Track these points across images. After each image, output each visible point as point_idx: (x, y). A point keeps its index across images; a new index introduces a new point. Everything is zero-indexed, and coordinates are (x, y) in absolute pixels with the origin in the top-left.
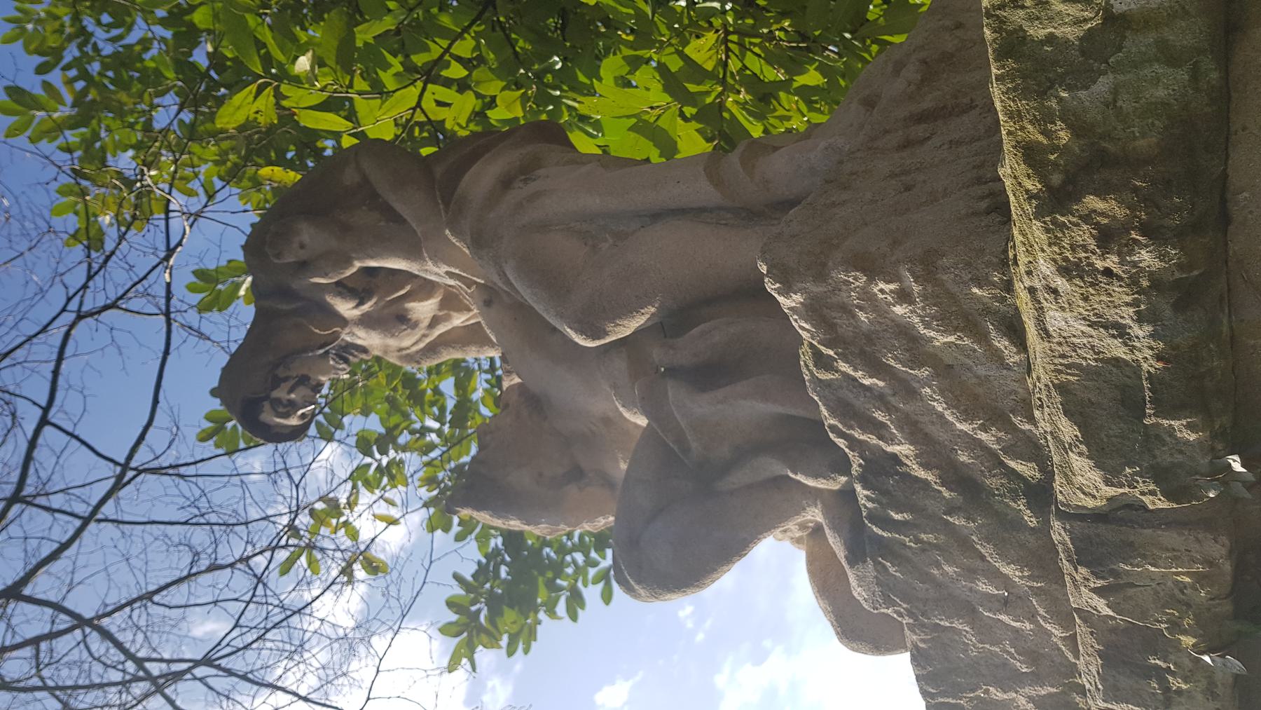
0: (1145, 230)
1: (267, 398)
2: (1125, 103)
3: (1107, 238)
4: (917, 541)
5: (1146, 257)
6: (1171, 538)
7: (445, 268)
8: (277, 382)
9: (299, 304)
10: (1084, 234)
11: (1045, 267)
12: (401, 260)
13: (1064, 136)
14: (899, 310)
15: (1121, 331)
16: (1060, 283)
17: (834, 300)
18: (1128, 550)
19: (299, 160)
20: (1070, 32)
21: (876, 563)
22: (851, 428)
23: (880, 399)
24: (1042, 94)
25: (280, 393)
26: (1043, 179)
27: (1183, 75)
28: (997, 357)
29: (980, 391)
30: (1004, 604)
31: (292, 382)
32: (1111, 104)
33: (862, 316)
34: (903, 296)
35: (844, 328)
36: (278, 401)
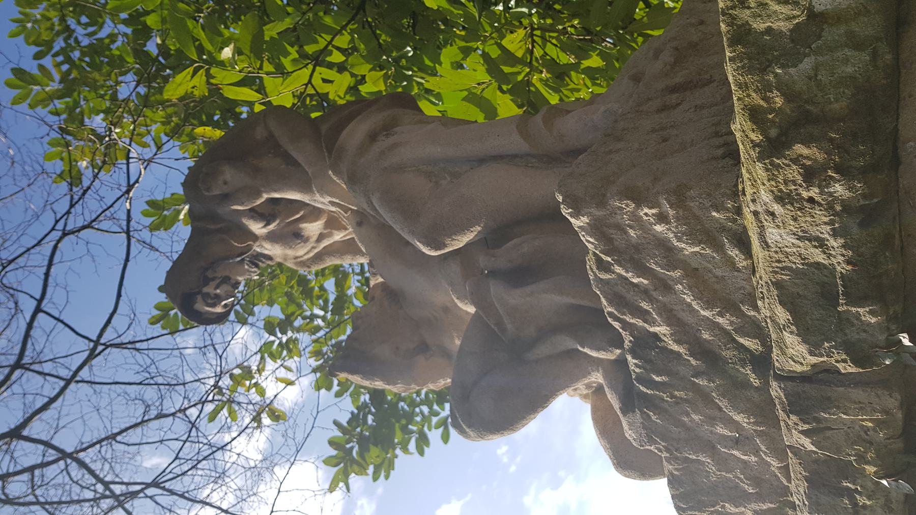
1: (199, 292)
2: (823, 77)
4: (672, 396)
5: (839, 189)
8: (206, 281)
10: (794, 173)
11: (765, 197)
12: (296, 193)
13: (779, 101)
14: (659, 228)
15: (821, 244)
16: (777, 208)
17: (612, 221)
18: (827, 403)
20: (783, 26)
21: (642, 413)
23: (645, 293)
24: (763, 70)
25: (209, 289)
26: (764, 132)
27: (866, 57)
29: (717, 287)
30: (736, 443)
31: (217, 281)
33: (632, 233)
34: (662, 218)
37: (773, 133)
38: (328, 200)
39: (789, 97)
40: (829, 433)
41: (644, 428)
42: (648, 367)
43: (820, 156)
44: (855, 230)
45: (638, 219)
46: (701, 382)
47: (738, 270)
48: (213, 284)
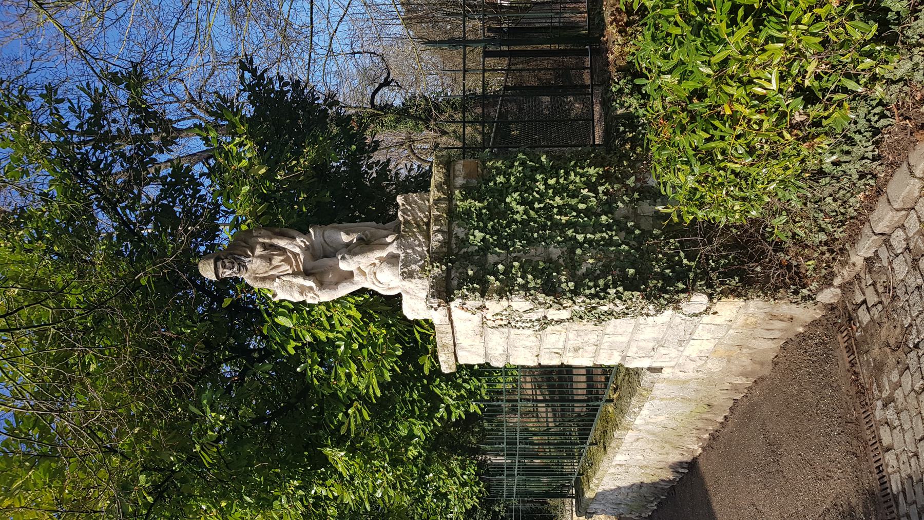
7: (302, 239)
30: (419, 245)
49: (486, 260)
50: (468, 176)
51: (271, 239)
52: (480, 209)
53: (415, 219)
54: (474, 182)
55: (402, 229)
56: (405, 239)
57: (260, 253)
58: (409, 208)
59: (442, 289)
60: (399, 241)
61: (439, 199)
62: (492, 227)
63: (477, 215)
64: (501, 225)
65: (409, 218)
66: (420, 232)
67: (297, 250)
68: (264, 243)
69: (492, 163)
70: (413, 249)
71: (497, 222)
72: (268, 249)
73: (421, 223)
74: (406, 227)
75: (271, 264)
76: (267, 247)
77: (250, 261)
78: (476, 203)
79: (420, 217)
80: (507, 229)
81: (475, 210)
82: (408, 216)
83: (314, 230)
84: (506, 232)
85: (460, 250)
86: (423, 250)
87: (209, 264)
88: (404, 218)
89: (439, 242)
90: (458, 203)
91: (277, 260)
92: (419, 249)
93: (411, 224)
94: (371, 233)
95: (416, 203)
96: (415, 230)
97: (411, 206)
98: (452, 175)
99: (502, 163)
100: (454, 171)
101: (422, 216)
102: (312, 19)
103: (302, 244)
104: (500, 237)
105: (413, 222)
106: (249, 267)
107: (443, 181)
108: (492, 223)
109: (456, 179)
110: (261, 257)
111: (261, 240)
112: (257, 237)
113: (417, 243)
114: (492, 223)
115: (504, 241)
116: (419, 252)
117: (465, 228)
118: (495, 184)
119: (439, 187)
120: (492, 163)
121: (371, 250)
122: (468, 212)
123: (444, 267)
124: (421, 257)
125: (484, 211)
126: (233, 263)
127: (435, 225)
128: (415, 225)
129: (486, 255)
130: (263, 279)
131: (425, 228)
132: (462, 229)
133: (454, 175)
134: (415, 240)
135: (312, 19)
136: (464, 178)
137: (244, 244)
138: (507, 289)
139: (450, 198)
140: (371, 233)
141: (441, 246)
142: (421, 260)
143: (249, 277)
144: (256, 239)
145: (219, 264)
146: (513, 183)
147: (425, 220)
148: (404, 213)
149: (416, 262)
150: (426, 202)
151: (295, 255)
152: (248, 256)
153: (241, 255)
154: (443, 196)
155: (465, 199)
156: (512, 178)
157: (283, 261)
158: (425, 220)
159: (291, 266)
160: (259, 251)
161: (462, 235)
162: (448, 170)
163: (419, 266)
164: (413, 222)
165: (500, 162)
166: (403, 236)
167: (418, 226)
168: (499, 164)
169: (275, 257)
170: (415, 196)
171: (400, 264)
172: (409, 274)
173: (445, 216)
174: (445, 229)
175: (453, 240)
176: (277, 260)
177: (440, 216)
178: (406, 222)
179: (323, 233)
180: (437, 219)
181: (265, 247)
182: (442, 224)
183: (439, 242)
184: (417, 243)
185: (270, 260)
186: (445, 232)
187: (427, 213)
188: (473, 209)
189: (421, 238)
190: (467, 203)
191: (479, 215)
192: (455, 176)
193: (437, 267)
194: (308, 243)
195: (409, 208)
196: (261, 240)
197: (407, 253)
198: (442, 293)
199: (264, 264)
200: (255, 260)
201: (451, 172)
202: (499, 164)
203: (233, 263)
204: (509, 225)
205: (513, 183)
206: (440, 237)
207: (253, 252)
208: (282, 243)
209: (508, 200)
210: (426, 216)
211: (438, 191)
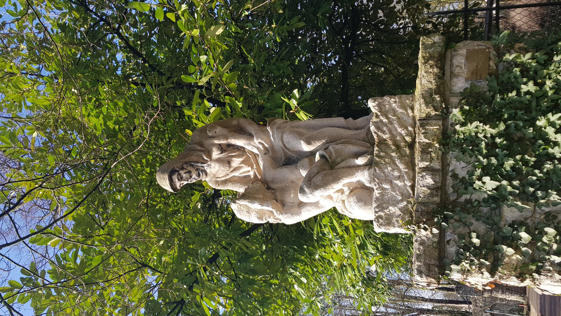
0: (435, 66)
1: (178, 171)
2: (435, 51)
3: (431, 67)
4: (385, 161)
5: (435, 70)
6: (434, 122)
7: (260, 141)
8: (183, 169)
9: (203, 149)
10: (428, 66)
11: (423, 72)
12: (242, 140)
13: (428, 55)
14: (394, 105)
15: (431, 82)
16: (425, 74)
17: (383, 104)
18: (427, 124)
19: (279, 78)
20: (430, 43)
21: (375, 169)
22: (378, 131)
23: (386, 125)
24: (426, 50)
25: (182, 172)
26: (425, 60)
27: (441, 48)
28: (408, 114)
29: (404, 123)
30: (399, 178)
31: (187, 171)
32: (433, 51)
33: (387, 106)
34: (395, 102)
35: (383, 110)
36: (180, 174)
37: (426, 61)
38: (259, 141)
39: (429, 54)
40: (427, 134)
41: (373, 175)
42: (380, 151)
43: (433, 63)
44: (437, 79)
45: (389, 102)
46: (393, 154)
47: (410, 117)
48: (185, 171)
49: (500, 215)
50: (475, 75)
51: (227, 138)
52: (493, 137)
53: (393, 138)
54: (483, 85)
55: (375, 152)
56: (380, 168)
57: (217, 157)
58: (385, 120)
59: (433, 262)
60: (372, 170)
61: (428, 117)
62: (511, 168)
63: (487, 144)
64: (526, 163)
65: (385, 137)
66: (402, 157)
67: (256, 151)
68: (220, 145)
69: (513, 56)
70: (391, 183)
71: (521, 160)
72: (225, 151)
73: (402, 144)
74: (381, 150)
75: (230, 167)
76: (224, 148)
77: (208, 165)
78: (487, 127)
79: (401, 134)
80: (537, 171)
81: (485, 137)
82: (384, 132)
83: (271, 128)
84: (535, 175)
85: (459, 196)
86: (405, 185)
87: (164, 179)
88: (378, 136)
89: (429, 188)
90: (458, 127)
91: (236, 162)
92: (398, 183)
93: (387, 145)
94: (336, 151)
95: (394, 112)
96: (393, 154)
97: (387, 118)
98: (447, 73)
99: (533, 58)
100: (451, 65)
101: (403, 132)
102: (18, 234)
103: (261, 147)
104: (524, 184)
105: (390, 142)
106: (208, 171)
107: (433, 86)
108: (511, 162)
109: (455, 80)
110: (219, 161)
111: (217, 142)
112: (213, 137)
113: (396, 174)
114: (511, 162)
115: (532, 189)
116: (399, 187)
117: (468, 163)
118: (518, 94)
119: (428, 98)
120: (513, 56)
121: (336, 179)
122: (473, 141)
123: (435, 231)
124: (402, 195)
125: (498, 140)
126: (189, 172)
127: (422, 160)
128: (393, 147)
129: (499, 207)
130: (225, 182)
131: (408, 152)
132: (463, 164)
133: (452, 72)
134: (393, 170)
135: (18, 234)
136: (467, 80)
137: (199, 148)
138: (534, 268)
139: (445, 115)
140: (336, 151)
141: (431, 195)
142: (402, 201)
143: (211, 181)
144: (212, 142)
145: (175, 178)
146: (550, 93)
147: (408, 139)
148: (378, 128)
149: (395, 203)
150: (410, 111)
151: (255, 155)
152: (205, 162)
153: (197, 162)
154: (433, 113)
155: (468, 118)
156: (549, 83)
157: (243, 162)
158: (408, 139)
159: (252, 168)
160: (216, 154)
161: (462, 173)
162: (442, 69)
163: (400, 209)
164: (390, 142)
165: (528, 55)
166: (377, 164)
167: (398, 148)
168: (526, 58)
169: (234, 159)
170: (392, 102)
171: (374, 205)
172: (387, 219)
173: (437, 145)
174: (437, 165)
175: (450, 181)
176: (236, 162)
177: (429, 145)
178: (382, 142)
179: (282, 137)
180: (425, 150)
181: (222, 149)
182: (432, 158)
183: (429, 188)
184: (396, 174)
185: (229, 163)
186: (437, 170)
187: (410, 129)
188: (480, 136)
189: (401, 166)
190: (471, 127)
191: (492, 145)
192: (453, 75)
193: (425, 229)
194: (266, 145)
195: (385, 120)
196: (217, 142)
197: (383, 189)
198: (432, 268)
199: (223, 168)
200: (213, 164)
201: (447, 68)
202: (526, 58)
203: (189, 172)
204: (539, 165)
205: (550, 93)
206: (429, 181)
207: (209, 155)
208: (239, 142)
209: (541, 122)
210: (409, 134)
211: (427, 104)
